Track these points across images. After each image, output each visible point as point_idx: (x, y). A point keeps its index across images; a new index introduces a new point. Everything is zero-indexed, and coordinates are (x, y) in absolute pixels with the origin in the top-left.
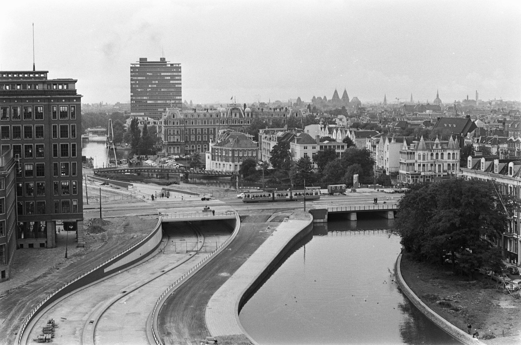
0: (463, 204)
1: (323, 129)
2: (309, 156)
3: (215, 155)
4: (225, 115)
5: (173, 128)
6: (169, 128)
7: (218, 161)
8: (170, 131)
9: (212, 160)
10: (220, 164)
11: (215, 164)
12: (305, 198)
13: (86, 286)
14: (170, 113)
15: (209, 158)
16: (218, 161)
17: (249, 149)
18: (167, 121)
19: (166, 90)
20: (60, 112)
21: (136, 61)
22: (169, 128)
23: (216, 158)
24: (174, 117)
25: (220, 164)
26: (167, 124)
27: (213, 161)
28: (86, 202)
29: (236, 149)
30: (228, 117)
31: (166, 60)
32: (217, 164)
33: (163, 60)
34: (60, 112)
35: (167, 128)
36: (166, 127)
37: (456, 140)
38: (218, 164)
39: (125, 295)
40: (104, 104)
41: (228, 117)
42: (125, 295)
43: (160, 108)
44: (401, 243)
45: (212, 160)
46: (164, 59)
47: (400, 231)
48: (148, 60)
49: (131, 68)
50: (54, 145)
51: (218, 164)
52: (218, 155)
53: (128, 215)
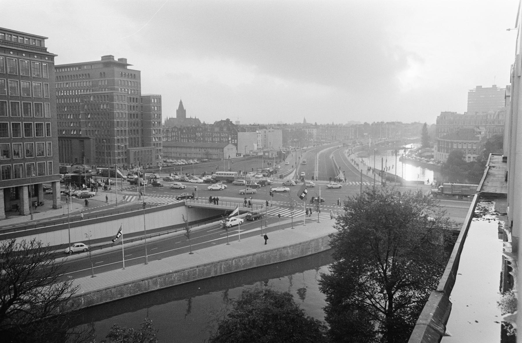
2: (406, 146)
4: (492, 117)
13: (132, 248)
15: (270, 143)
17: (468, 141)
21: (473, 87)
25: (442, 155)
28: (374, 178)
29: (455, 141)
30: (495, 118)
31: (497, 86)
32: (440, 154)
33: (494, 86)
41: (495, 118)
43: (157, 101)
46: (496, 85)
47: (292, 305)
48: (483, 87)
49: (469, 93)
50: (12, 123)
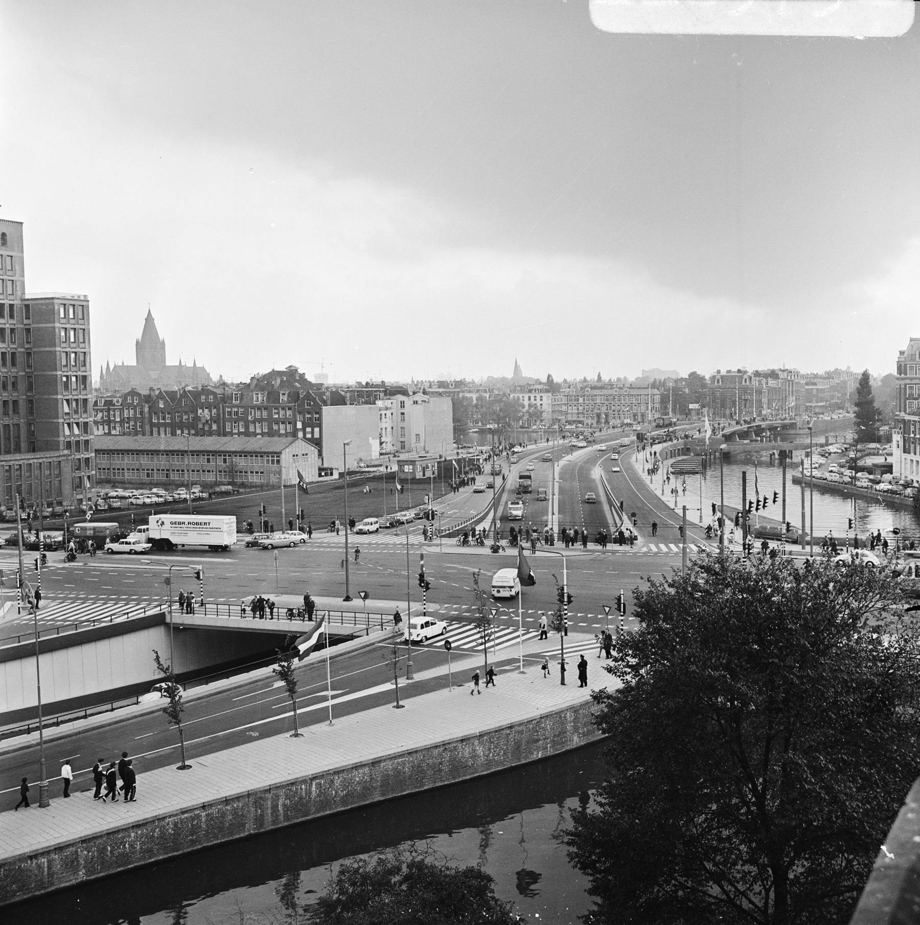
0: (692, 454)
3: (909, 438)
7: (915, 454)
8: (911, 388)
11: (909, 462)
12: (856, 539)
16: (915, 454)
18: (906, 365)
22: (908, 381)
26: (906, 374)
32: (912, 461)
35: (903, 382)
36: (903, 379)
37: (672, 591)
38: (915, 462)
39: (784, 501)
42: (784, 501)
44: (693, 375)
45: (904, 452)
51: (915, 462)
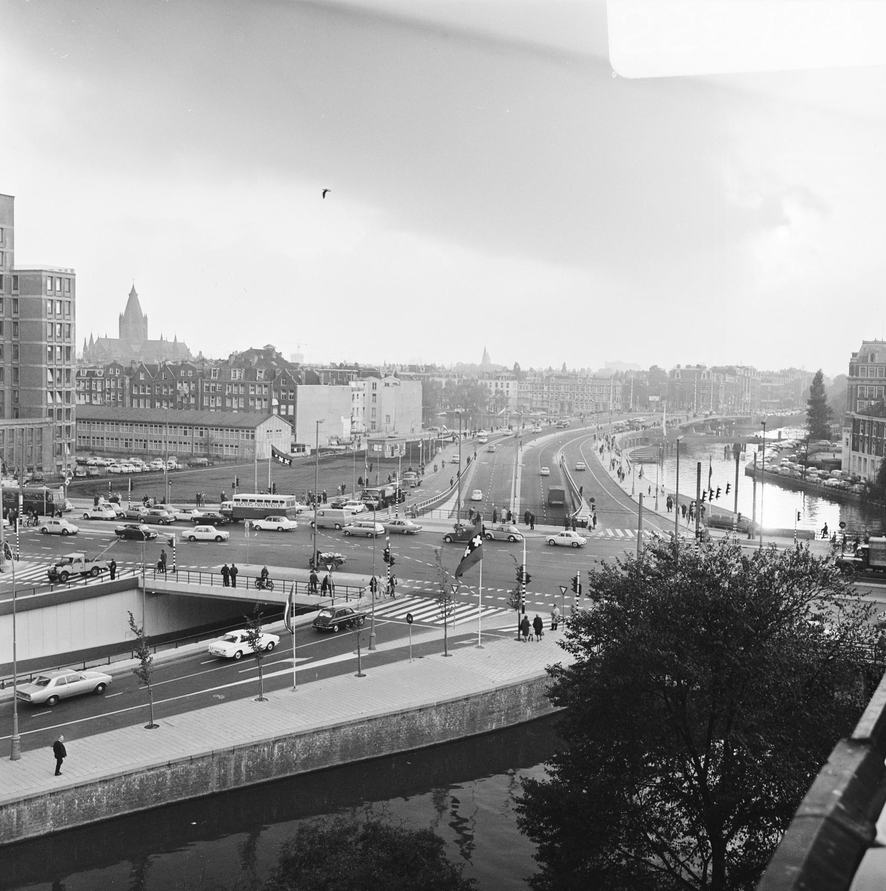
1: (391, 475)
5: (868, 383)
6: (859, 382)
8: (862, 389)
9: (853, 449)
10: (865, 460)
14: (867, 350)
16: (863, 452)
18: (857, 367)
19: (220, 645)
20: (855, 557)
22: (859, 382)
23: (861, 444)
24: (872, 359)
25: (865, 460)
26: (857, 375)
27: (855, 453)
32: (860, 458)
34: (855, 557)
35: (854, 383)
38: (863, 460)
40: (683, 367)
45: (853, 449)
51: (863, 460)
52: (863, 437)
53: (630, 432)
